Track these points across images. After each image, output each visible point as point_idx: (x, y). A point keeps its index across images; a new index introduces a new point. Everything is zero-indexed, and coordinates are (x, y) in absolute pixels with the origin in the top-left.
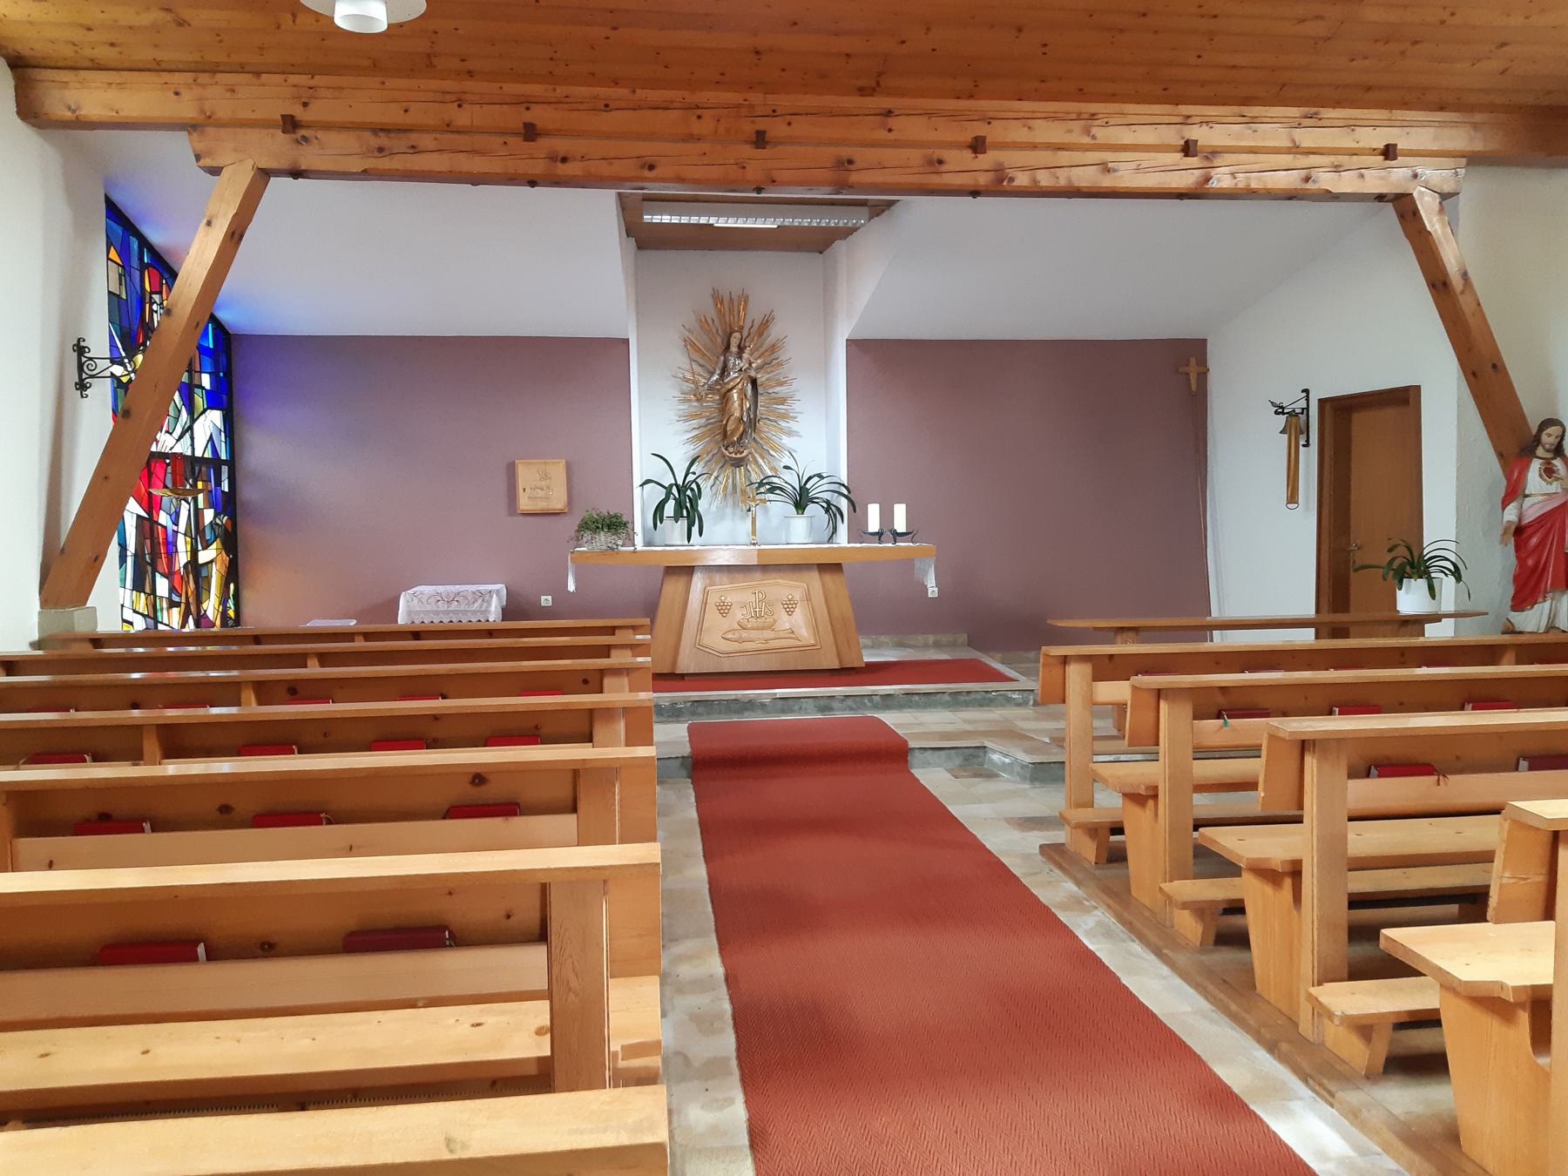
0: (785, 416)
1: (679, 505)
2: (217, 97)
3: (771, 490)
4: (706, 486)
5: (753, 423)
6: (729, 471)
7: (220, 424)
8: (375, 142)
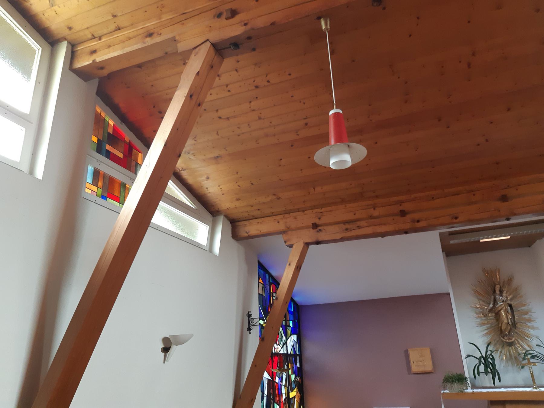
0: (529, 320)
1: (486, 366)
2: (290, 221)
3: (533, 357)
4: (496, 356)
5: (514, 324)
6: (506, 348)
7: (296, 340)
8: (344, 227)
